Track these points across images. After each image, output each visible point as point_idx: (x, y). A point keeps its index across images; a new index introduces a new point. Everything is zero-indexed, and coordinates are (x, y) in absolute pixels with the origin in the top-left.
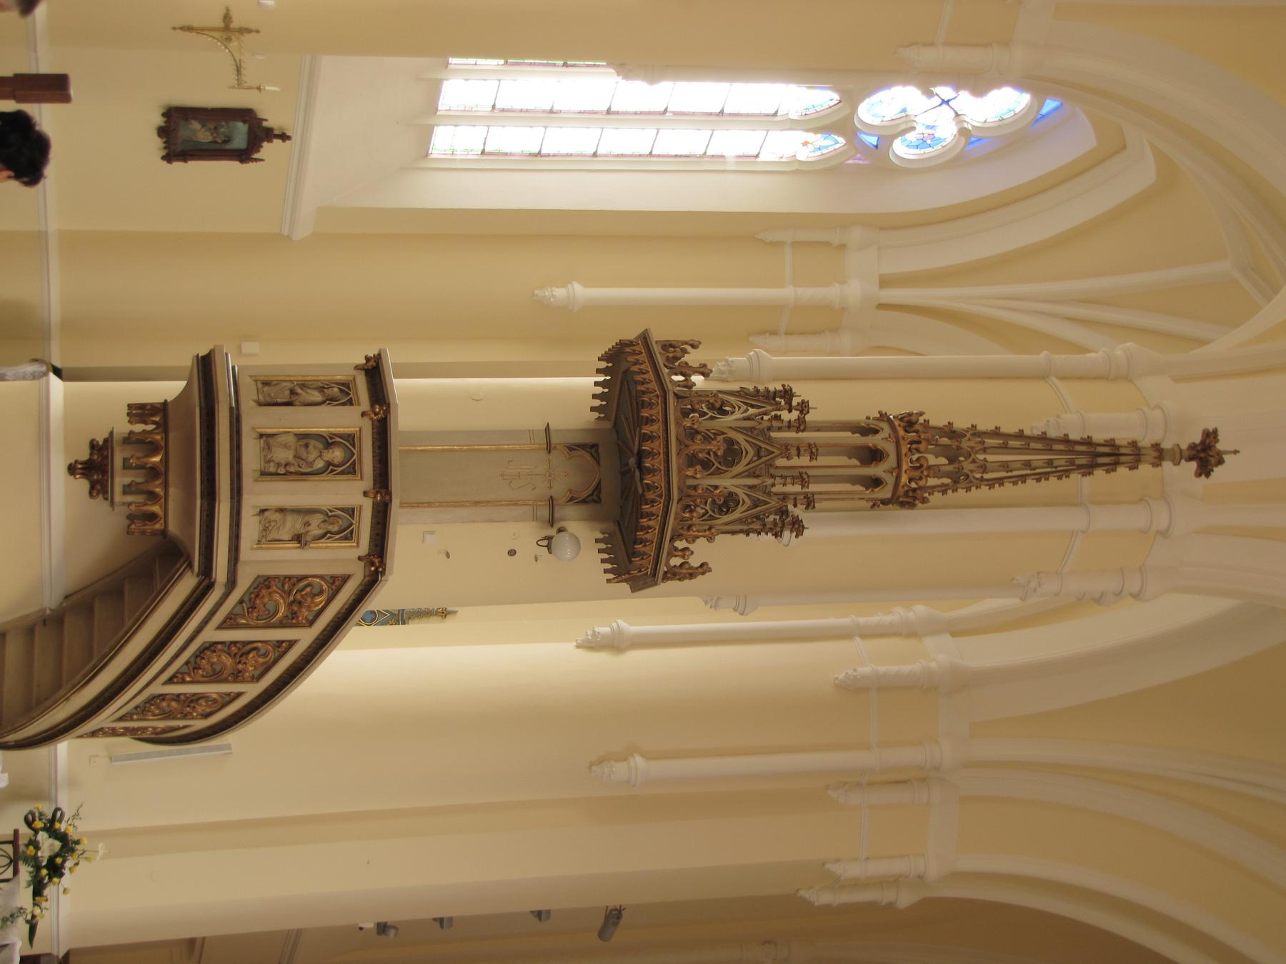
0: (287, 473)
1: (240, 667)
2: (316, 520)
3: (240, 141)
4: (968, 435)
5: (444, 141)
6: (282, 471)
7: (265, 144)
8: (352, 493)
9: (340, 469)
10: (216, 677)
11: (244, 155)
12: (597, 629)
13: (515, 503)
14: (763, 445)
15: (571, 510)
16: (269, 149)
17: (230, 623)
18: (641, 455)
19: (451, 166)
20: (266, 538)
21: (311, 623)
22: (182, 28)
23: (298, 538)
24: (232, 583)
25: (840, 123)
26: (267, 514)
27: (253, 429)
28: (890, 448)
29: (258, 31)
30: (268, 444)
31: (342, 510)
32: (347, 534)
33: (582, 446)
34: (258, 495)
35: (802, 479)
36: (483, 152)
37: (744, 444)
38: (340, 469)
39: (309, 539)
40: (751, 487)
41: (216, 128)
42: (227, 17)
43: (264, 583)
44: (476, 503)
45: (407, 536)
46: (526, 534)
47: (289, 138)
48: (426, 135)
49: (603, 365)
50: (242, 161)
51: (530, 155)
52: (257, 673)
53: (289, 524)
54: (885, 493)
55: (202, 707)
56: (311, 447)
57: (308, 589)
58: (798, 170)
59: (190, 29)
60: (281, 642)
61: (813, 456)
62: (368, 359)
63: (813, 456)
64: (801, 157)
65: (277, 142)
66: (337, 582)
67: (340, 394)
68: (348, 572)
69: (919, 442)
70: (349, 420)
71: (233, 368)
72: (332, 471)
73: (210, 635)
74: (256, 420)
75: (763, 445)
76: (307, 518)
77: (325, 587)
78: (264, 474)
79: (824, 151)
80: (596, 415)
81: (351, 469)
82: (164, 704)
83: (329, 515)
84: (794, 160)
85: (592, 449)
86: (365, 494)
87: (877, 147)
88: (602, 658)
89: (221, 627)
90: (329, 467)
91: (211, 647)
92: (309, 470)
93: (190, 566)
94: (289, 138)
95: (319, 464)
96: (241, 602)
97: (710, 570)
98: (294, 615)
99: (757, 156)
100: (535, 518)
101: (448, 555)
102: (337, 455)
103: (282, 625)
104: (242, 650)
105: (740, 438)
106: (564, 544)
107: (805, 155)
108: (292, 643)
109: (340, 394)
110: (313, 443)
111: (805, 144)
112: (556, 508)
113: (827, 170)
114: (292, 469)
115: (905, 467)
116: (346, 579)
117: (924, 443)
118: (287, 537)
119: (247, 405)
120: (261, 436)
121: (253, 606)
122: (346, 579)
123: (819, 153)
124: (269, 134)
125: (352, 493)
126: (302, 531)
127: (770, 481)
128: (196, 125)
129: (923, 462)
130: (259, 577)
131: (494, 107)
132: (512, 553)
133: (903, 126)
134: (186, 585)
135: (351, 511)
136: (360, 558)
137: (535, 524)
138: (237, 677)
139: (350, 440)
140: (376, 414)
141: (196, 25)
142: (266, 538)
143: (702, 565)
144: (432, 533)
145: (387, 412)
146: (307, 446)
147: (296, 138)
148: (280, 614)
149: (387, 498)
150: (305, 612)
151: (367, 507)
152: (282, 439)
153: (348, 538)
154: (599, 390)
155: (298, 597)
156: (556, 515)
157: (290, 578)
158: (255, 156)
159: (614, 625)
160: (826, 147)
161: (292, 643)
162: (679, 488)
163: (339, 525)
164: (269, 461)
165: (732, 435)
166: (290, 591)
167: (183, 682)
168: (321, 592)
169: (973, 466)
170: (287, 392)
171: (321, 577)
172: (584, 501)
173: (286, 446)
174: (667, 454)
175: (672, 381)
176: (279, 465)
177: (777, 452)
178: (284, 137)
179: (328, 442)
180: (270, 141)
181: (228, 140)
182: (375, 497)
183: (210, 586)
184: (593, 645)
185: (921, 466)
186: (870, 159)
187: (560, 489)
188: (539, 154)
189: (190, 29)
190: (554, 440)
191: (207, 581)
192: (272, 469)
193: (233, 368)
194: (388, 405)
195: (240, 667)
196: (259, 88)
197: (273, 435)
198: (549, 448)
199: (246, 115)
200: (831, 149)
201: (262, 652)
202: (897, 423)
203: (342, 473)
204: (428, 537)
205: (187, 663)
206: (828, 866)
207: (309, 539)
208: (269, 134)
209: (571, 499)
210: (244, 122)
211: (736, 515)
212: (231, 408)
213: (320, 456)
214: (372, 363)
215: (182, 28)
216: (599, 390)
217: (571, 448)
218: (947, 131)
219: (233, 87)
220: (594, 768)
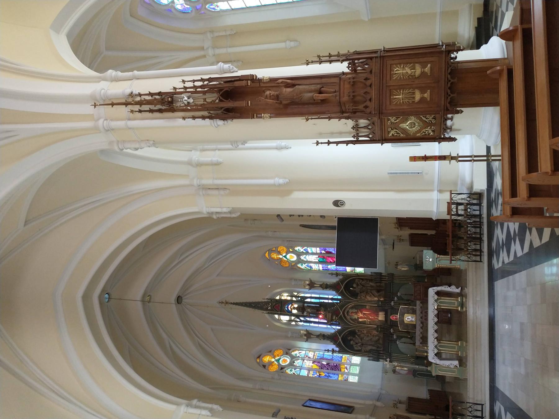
25: (293, 358)
58: (300, 349)
186: (287, 352)
206: (337, 349)
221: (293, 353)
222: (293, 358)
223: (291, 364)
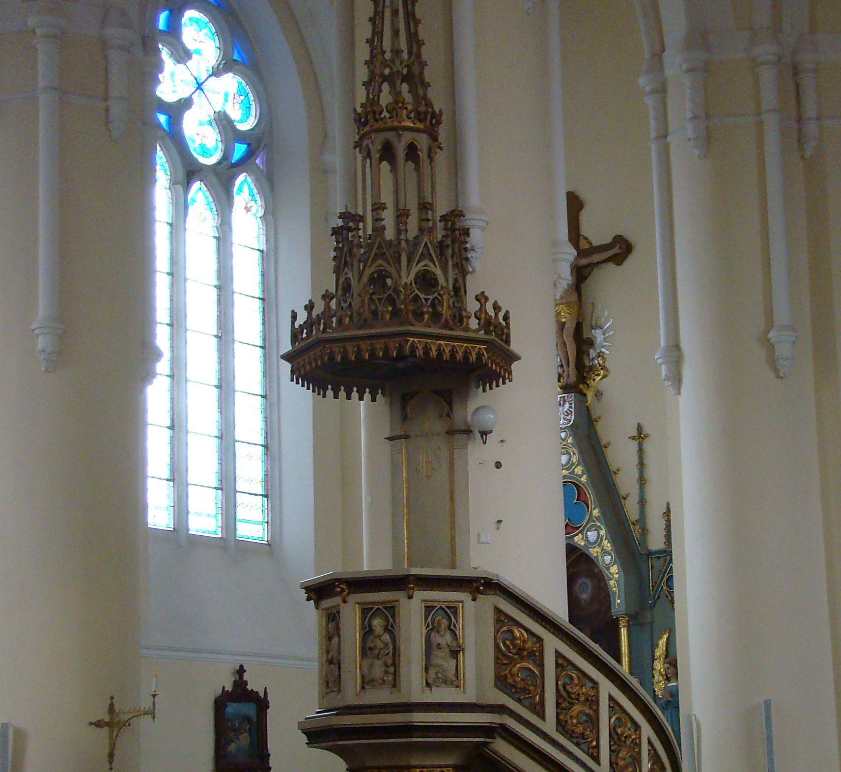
0: (394, 664)
1: (582, 699)
2: (437, 639)
3: (249, 709)
4: (372, 67)
5: (252, 526)
6: (392, 669)
7: (249, 687)
8: (412, 610)
9: (391, 620)
10: (593, 722)
11: (262, 704)
12: (664, 377)
13: (452, 464)
14: (374, 252)
15: (458, 414)
16: (254, 684)
17: (539, 710)
18: (401, 357)
19: (275, 518)
20: (456, 681)
21: (540, 640)
22: (111, 763)
23: (455, 653)
24: (501, 709)
25: (221, 179)
26: (430, 681)
27: (357, 695)
28: (408, 137)
29: (112, 698)
30: (368, 683)
31: (426, 619)
32: (451, 612)
33: (404, 409)
34: (414, 685)
35: (402, 215)
36: (266, 496)
37: (373, 269)
38: (391, 620)
39: (455, 644)
40: (409, 261)
41: (235, 730)
42: (99, 724)
43: (502, 682)
44: (452, 498)
45: (479, 561)
46: (477, 454)
47: (241, 667)
48: (247, 548)
49: (330, 393)
50: (268, 707)
51: (266, 454)
52: (590, 685)
53: (439, 661)
54: (423, 141)
55: (626, 730)
56: (372, 645)
57: (508, 643)
58: (271, 217)
59: (111, 756)
60: (557, 665)
61: (383, 207)
62: (309, 599)
63: (383, 207)
64: (261, 213)
65: (246, 677)
66: (501, 617)
67: (333, 617)
68: (492, 608)
69: (374, 113)
70: (351, 615)
71: (318, 713)
72: (392, 626)
73: (549, 725)
74: (351, 695)
75: (374, 252)
76: (434, 647)
77: (505, 628)
78: (395, 685)
79: (255, 191)
80: (379, 396)
81: (391, 609)
82: (621, 763)
83: (432, 629)
84: (264, 218)
85: (405, 399)
86: (410, 597)
87: (249, 145)
88: (688, 372)
89: (543, 717)
90: (390, 629)
91: (561, 725)
92: (391, 647)
93: (485, 744)
94: (241, 667)
95: (387, 637)
96: (519, 701)
97: (483, 293)
98: (531, 654)
99: (262, 251)
100: (465, 446)
101: (499, 522)
102: (377, 623)
103: (541, 665)
104: (564, 699)
105: (368, 272)
106: (488, 418)
107: (258, 208)
108: (558, 654)
109: (333, 617)
110: (369, 644)
111: (248, 209)
112: (455, 428)
113: (269, 186)
114: (390, 661)
115: (396, 124)
116: (498, 611)
117: (375, 108)
118: (453, 662)
119: (339, 701)
120: (363, 688)
121: (527, 691)
122: (498, 611)
123: (257, 197)
124: (240, 683)
125: (412, 610)
126: (447, 650)
127: (403, 244)
128: (232, 747)
129: (390, 108)
130: (496, 686)
131: (217, 489)
132: (498, 465)
133: (223, 122)
134: (503, 748)
135: (429, 609)
136: (474, 599)
137: (469, 447)
138: (593, 702)
139: (367, 611)
140: (343, 590)
141: (107, 751)
142: (456, 681)
143: (478, 300)
144: (479, 535)
145: (340, 581)
146: (370, 649)
147: (241, 660)
148: (531, 666)
149: (411, 578)
150: (529, 645)
151: (421, 595)
152: (365, 669)
153: (455, 610)
154: (367, 396)
155: (514, 651)
156: (464, 428)
157: (497, 659)
158: (262, 695)
159: (659, 361)
160: (251, 190)
161: (558, 654)
162: (360, 329)
163: (442, 618)
164: (384, 681)
165: (365, 279)
166: (509, 657)
167: (597, 747)
168: (510, 631)
169: (398, 62)
170: (332, 666)
171: (497, 631)
172: (450, 405)
173: (371, 666)
174: (370, 337)
175: (307, 338)
176: (386, 672)
177: (379, 239)
178: (241, 671)
179: (367, 632)
180: (246, 683)
181: (247, 719)
182: (412, 588)
183: (503, 727)
184: (677, 380)
185: (394, 108)
186: (255, 152)
187: (440, 426)
188: (266, 446)
189: (111, 756)
190: (398, 432)
191: (499, 731)
192: (391, 678)
193: (318, 713)
194: (336, 580)
195: (582, 699)
196: (154, 696)
197: (363, 677)
198: (406, 437)
199: (221, 703)
200: (252, 186)
201: (568, 681)
202: (362, 132)
203: (393, 617)
204: (483, 539)
205: (577, 745)
207: (455, 644)
208: (240, 683)
209: (448, 415)
210: (226, 706)
211: (438, 272)
212: (336, 714)
213: (379, 636)
214: (312, 595)
215: (111, 763)
216: (367, 396)
217: (405, 418)
218: (231, 82)
219: (154, 718)
220: (781, 374)
221: (244, 187)
222: (221, 179)
223: (189, 171)
